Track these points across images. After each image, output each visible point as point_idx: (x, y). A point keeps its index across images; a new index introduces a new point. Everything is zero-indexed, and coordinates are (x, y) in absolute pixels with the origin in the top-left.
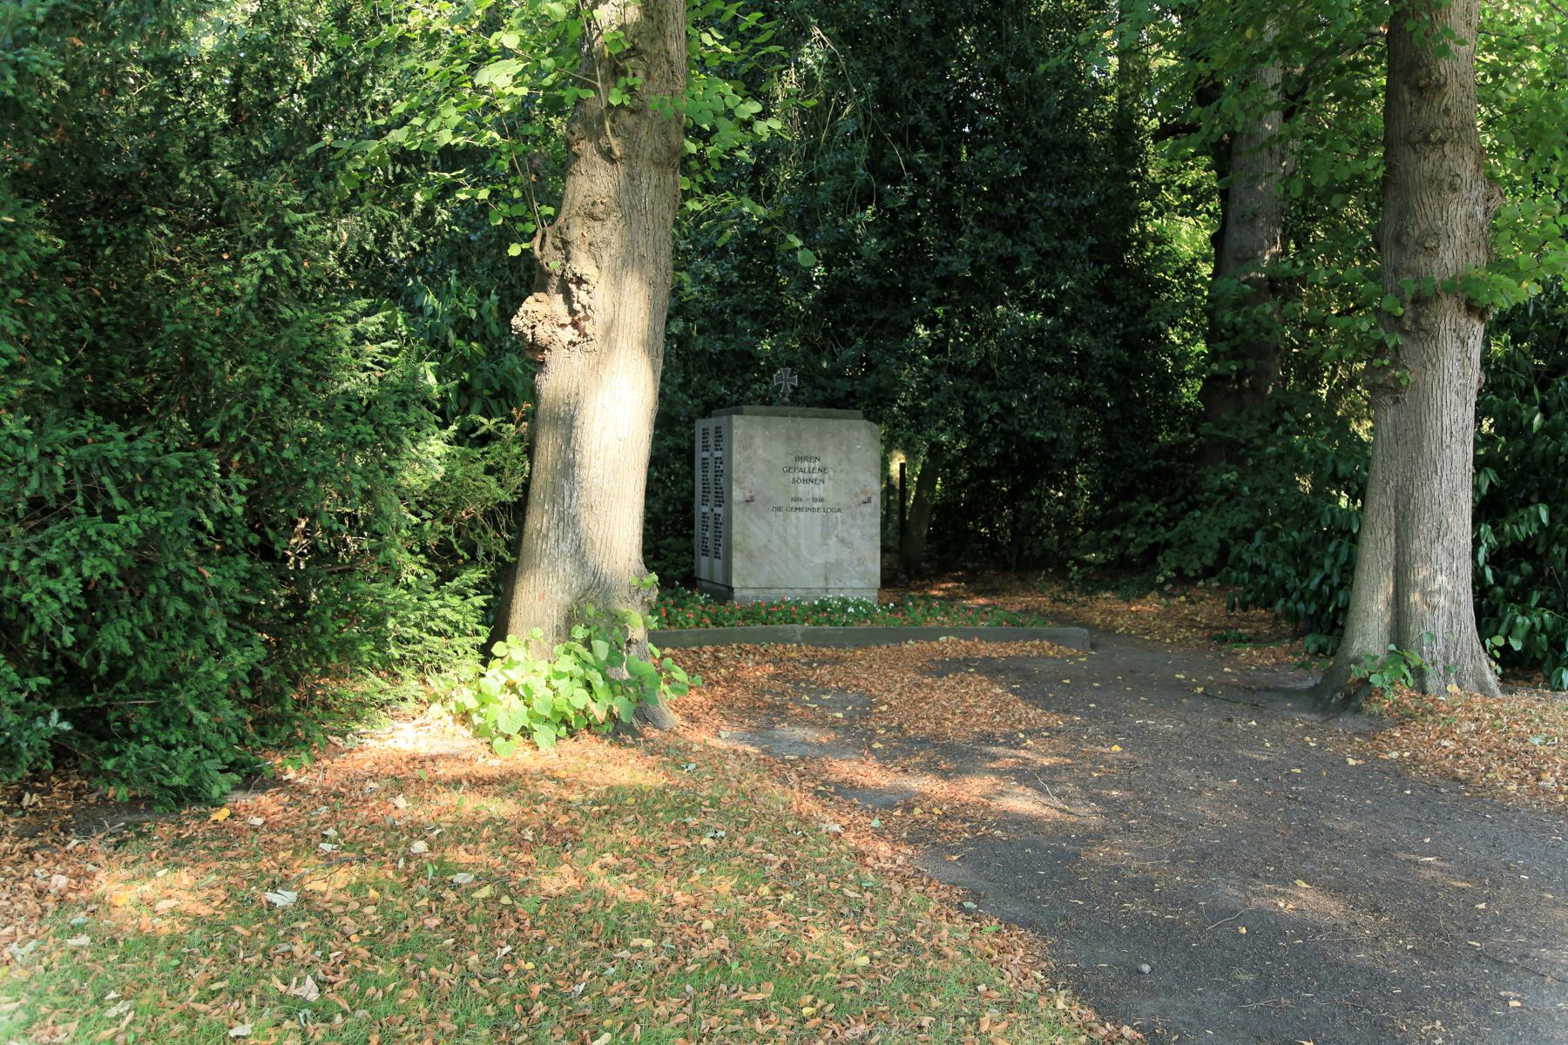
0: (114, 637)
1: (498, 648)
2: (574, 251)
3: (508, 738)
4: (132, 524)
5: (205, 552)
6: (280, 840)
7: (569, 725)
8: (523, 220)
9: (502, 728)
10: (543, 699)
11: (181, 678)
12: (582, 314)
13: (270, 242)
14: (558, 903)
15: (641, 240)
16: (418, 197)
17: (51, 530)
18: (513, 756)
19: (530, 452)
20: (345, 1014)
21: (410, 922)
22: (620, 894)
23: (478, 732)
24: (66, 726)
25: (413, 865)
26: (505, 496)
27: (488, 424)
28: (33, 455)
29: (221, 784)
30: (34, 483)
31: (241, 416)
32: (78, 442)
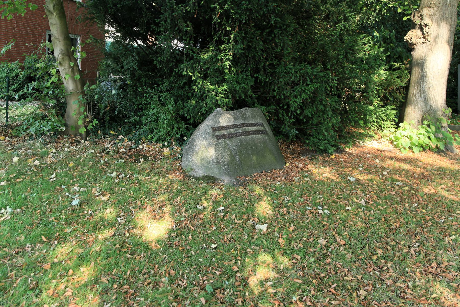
0: (307, 112)
1: (401, 124)
2: (424, 17)
3: (405, 149)
4: (312, 87)
5: (328, 94)
6: (348, 165)
7: (423, 148)
8: (407, 10)
9: (404, 146)
10: (415, 139)
11: (321, 124)
12: (426, 35)
13: (343, 21)
14: (430, 196)
15: (446, 12)
16: (378, 7)
17: (295, 88)
18: (406, 153)
19: (410, 73)
20: (374, 211)
21: (386, 192)
22: (450, 197)
23: (396, 146)
24: (297, 132)
25: (384, 177)
26: (403, 84)
27: (397, 65)
28: (293, 72)
29: (332, 150)
30: (293, 78)
31: (335, 63)
32: (301, 69)
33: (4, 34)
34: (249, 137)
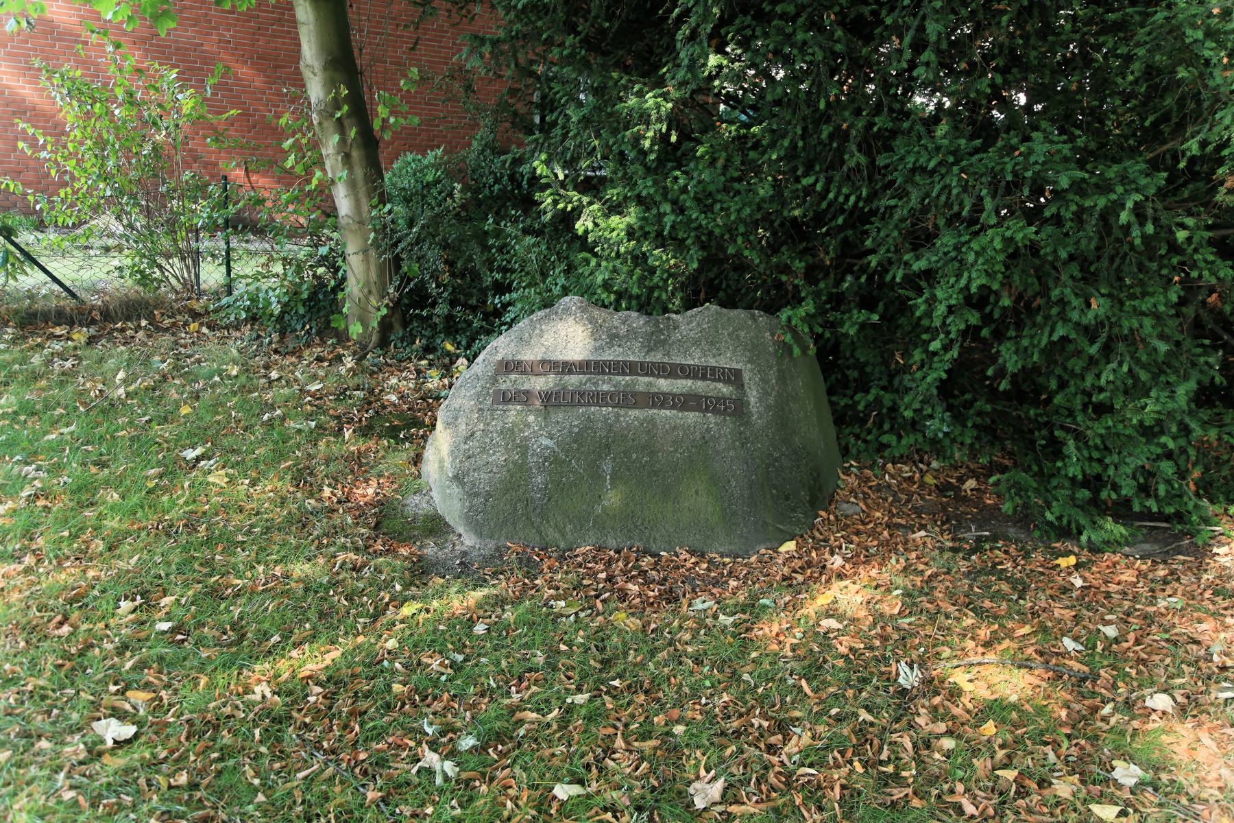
33: (164, 53)
34: (634, 413)
